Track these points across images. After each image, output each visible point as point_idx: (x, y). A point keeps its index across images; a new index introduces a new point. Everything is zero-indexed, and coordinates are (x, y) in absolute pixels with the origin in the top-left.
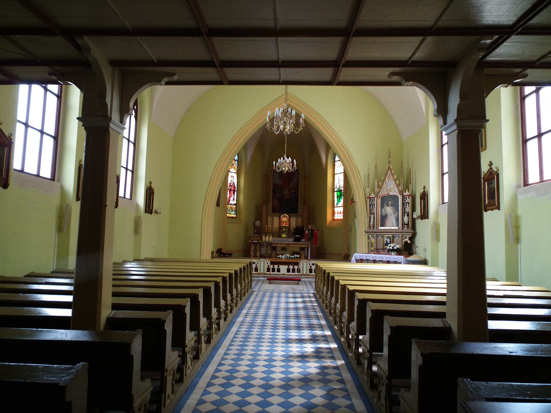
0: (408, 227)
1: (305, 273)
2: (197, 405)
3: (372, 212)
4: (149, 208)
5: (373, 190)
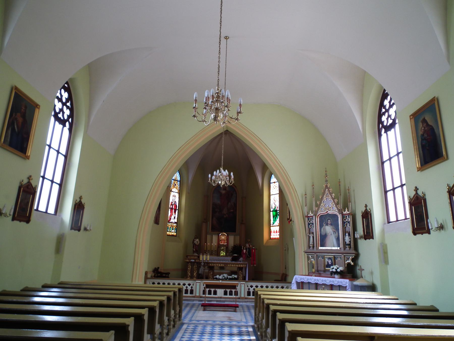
0: (350, 248)
1: (243, 296)
3: (311, 231)
4: (76, 224)
5: (311, 209)
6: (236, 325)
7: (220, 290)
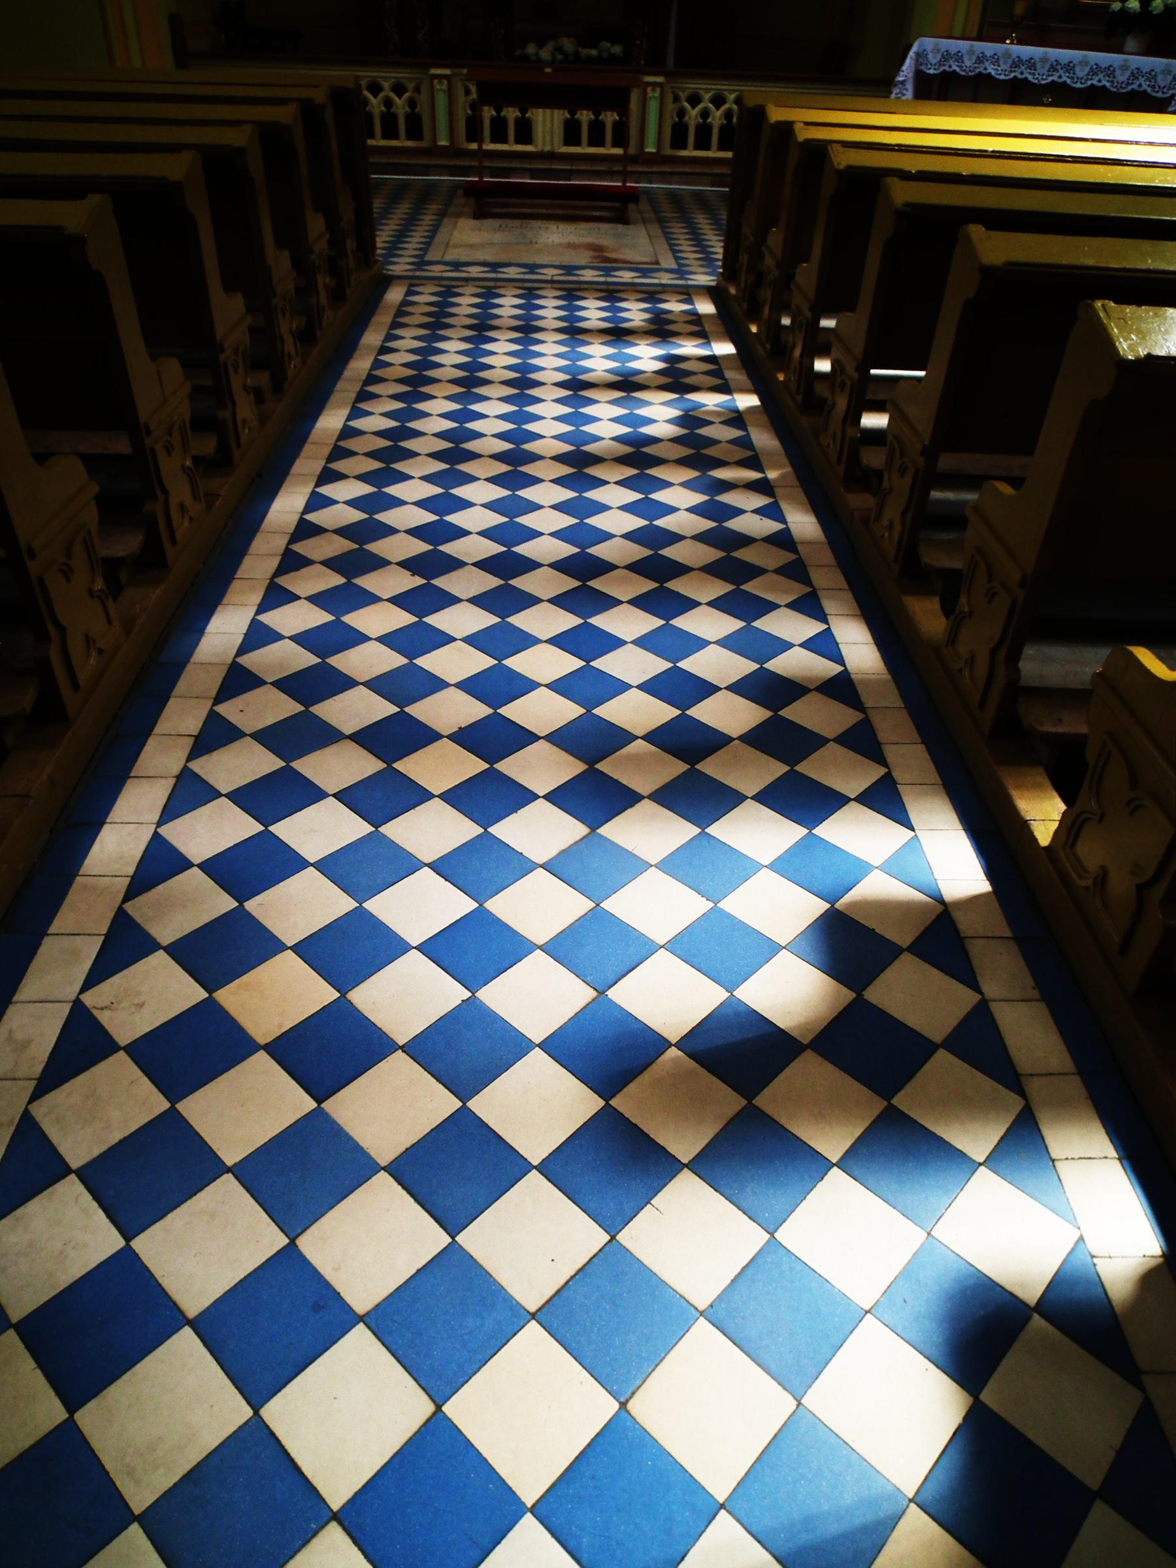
2: (243, 650)
6: (632, 287)
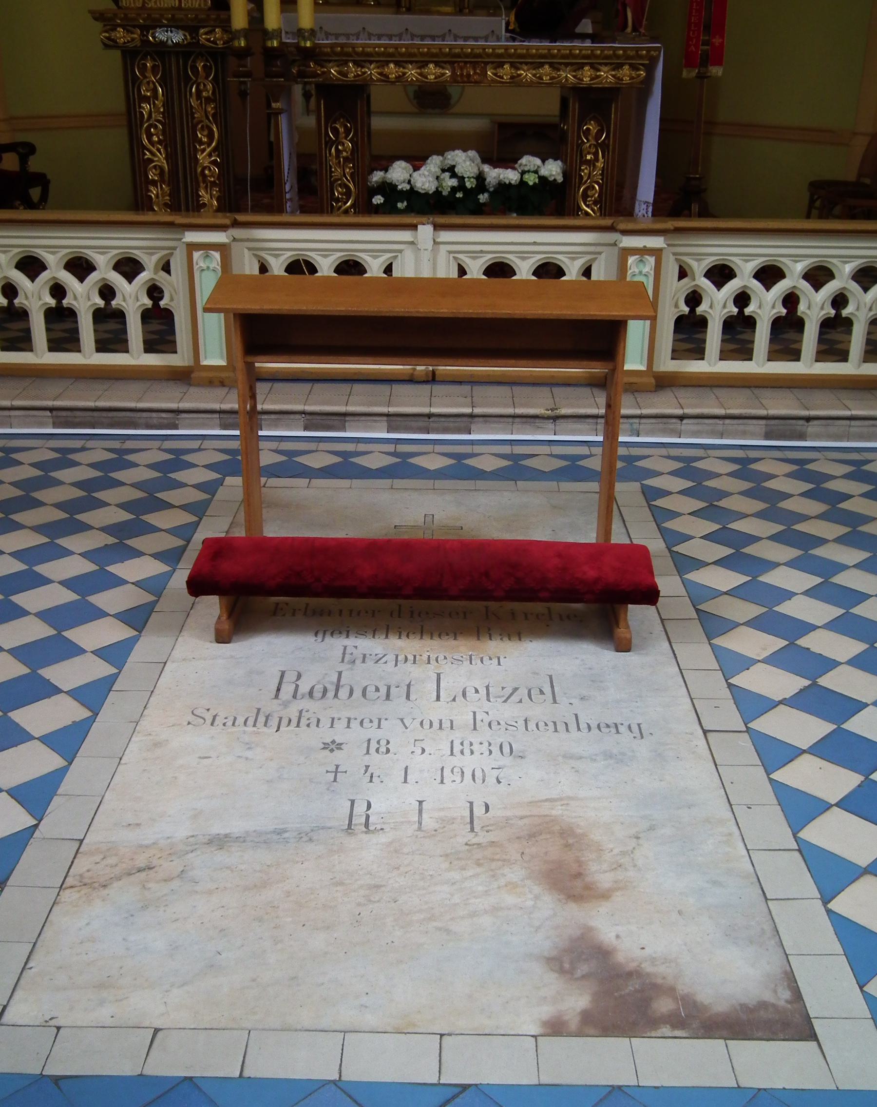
7: (407, 276)
